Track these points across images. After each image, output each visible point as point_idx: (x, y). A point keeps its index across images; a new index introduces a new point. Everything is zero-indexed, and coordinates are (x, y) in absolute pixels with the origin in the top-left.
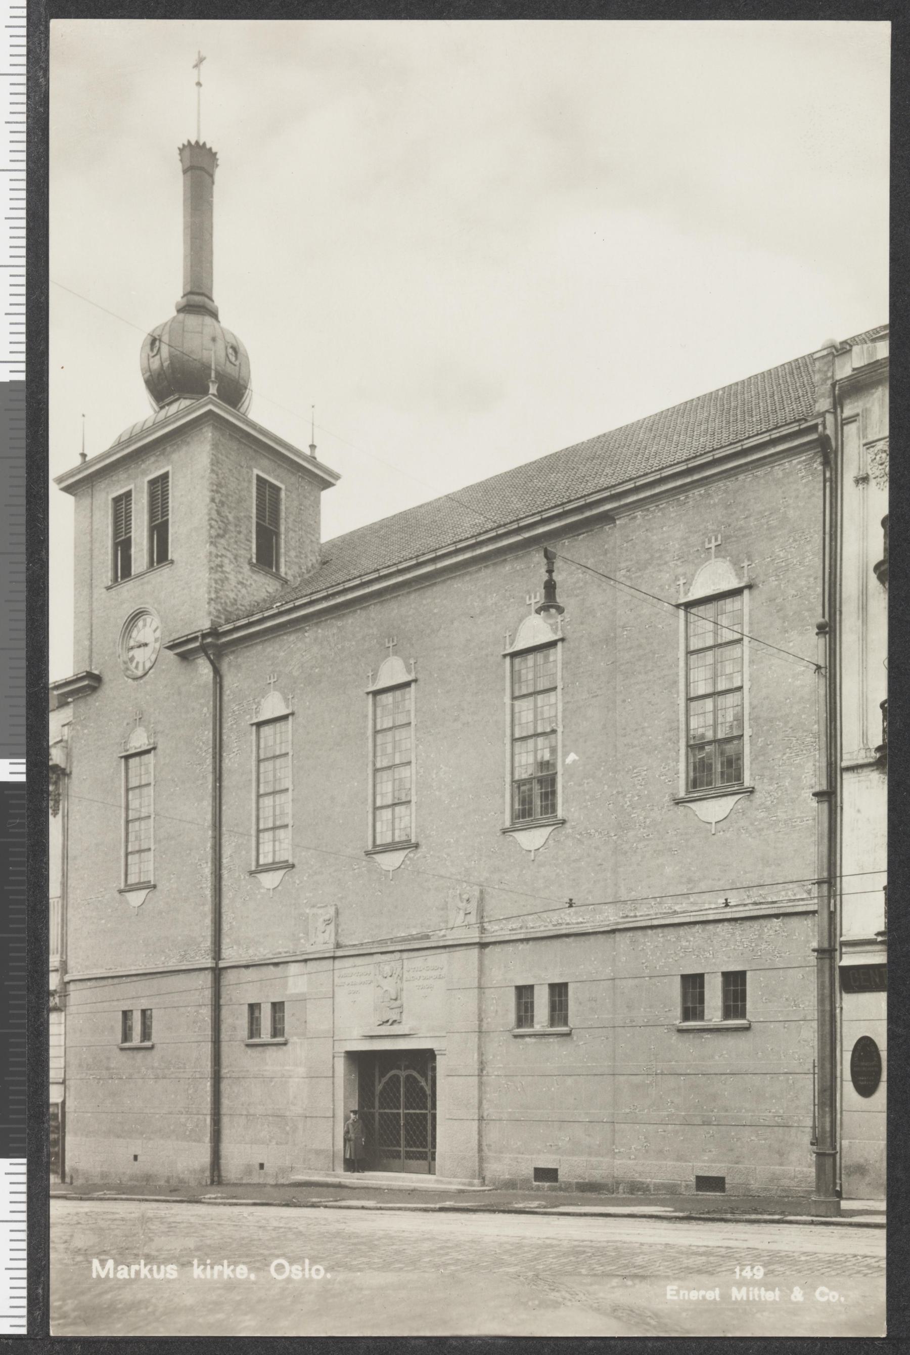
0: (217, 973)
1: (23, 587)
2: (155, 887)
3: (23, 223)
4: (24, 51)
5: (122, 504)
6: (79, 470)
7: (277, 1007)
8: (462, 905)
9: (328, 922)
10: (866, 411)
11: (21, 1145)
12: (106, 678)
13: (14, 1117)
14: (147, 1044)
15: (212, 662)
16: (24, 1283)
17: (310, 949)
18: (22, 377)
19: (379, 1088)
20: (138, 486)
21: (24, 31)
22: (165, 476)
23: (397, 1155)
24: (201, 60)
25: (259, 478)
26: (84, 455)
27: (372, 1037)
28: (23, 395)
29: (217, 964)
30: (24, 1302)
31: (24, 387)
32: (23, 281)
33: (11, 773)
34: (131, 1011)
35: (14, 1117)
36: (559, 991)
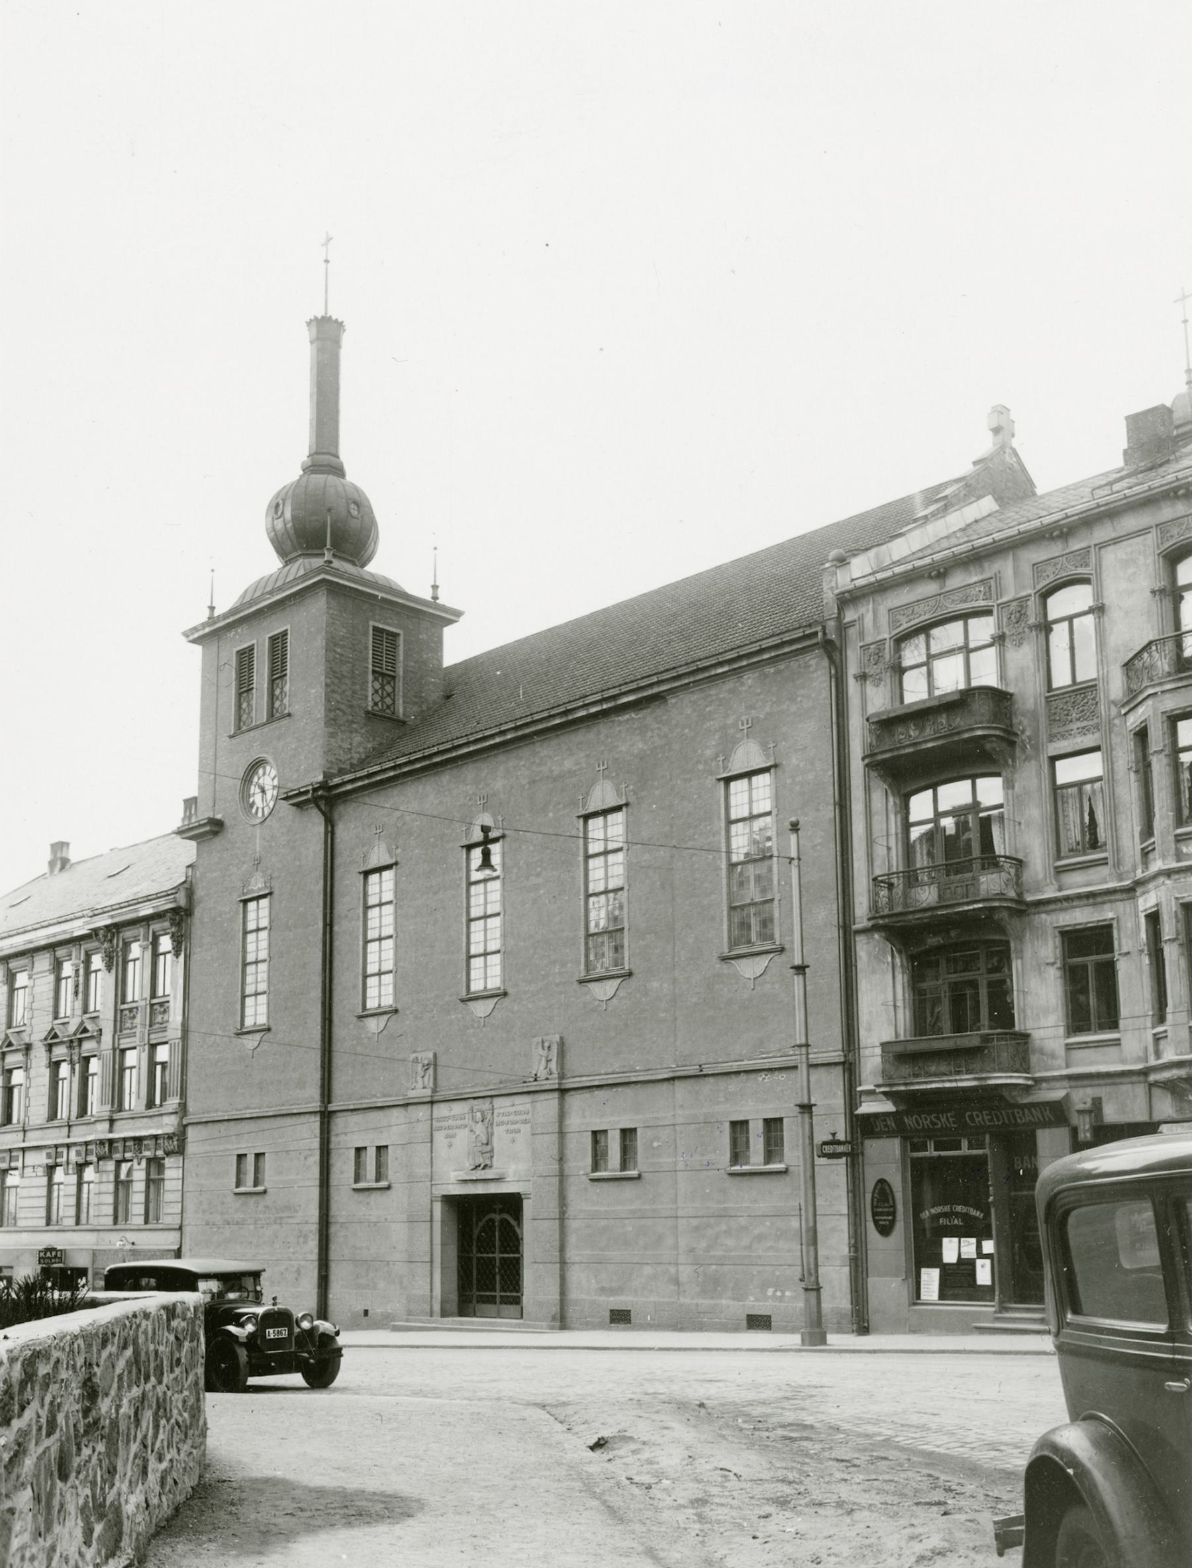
0: (326, 1117)
6: (204, 625)
9: (426, 1067)
10: (861, 618)
12: (227, 822)
15: (324, 813)
17: (412, 1094)
19: (476, 1231)
23: (491, 1300)
24: (329, 240)
25: (375, 629)
26: (212, 608)
27: (465, 1181)
34: (605, 1131)
36: (628, 1134)
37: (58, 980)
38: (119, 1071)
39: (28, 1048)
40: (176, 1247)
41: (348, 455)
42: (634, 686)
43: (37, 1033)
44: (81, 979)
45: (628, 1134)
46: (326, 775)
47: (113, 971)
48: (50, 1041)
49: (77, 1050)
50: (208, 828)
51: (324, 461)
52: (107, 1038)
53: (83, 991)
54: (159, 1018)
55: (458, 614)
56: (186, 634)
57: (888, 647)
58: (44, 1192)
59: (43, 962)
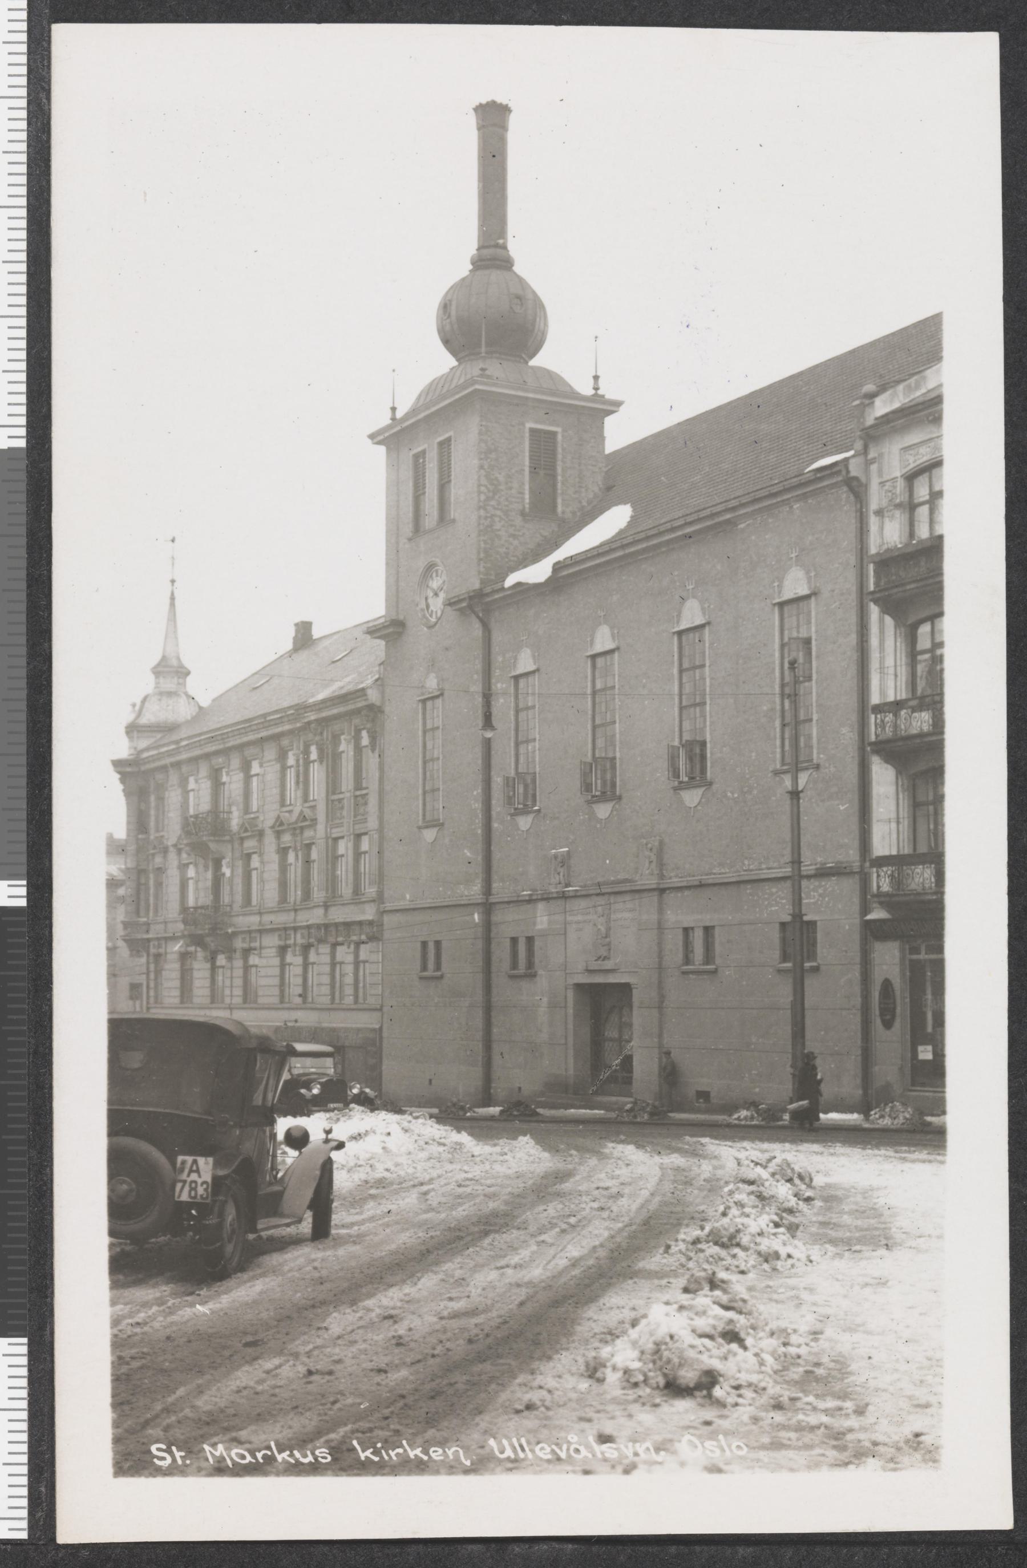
1: (23, 683)
2: (442, 824)
3: (24, 267)
4: (24, 70)
5: (419, 460)
7: (530, 940)
8: (647, 853)
11: (22, 1322)
13: (12, 1290)
14: (439, 973)
15: (481, 620)
16: (24, 1480)
18: (22, 443)
20: (429, 446)
21: (24, 48)
22: (449, 439)
28: (23, 464)
29: (487, 899)
30: (25, 1502)
31: (24, 455)
32: (23, 333)
33: (9, 897)
35: (12, 1290)
37: (284, 768)
38: (333, 858)
39: (261, 834)
40: (377, 1027)
41: (517, 246)
42: (707, 512)
43: (267, 820)
44: (301, 768)
45: (708, 930)
46: (482, 582)
47: (325, 763)
48: (277, 829)
49: (299, 838)
50: (391, 630)
51: (492, 255)
52: (321, 828)
53: (304, 781)
54: (361, 811)
55: (618, 404)
56: (372, 436)
57: (901, 484)
58: (277, 971)
59: (270, 753)
